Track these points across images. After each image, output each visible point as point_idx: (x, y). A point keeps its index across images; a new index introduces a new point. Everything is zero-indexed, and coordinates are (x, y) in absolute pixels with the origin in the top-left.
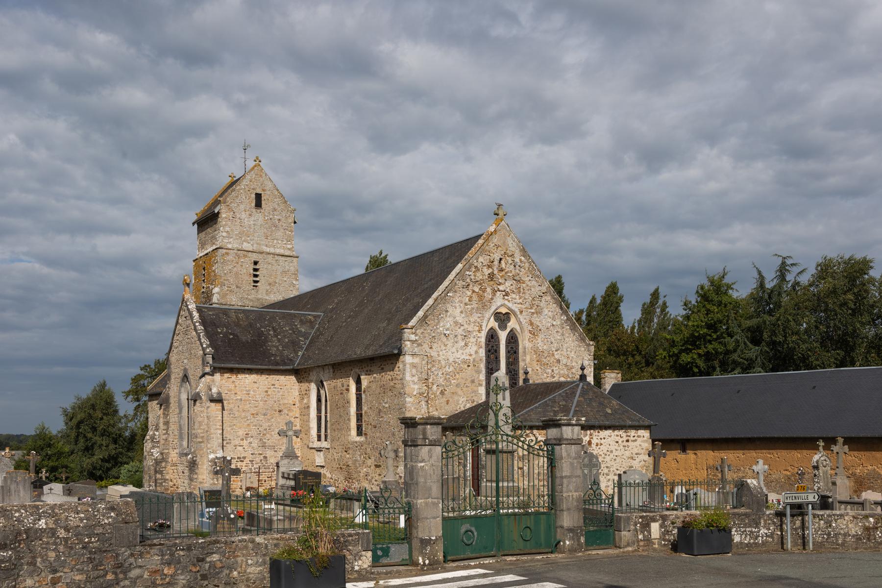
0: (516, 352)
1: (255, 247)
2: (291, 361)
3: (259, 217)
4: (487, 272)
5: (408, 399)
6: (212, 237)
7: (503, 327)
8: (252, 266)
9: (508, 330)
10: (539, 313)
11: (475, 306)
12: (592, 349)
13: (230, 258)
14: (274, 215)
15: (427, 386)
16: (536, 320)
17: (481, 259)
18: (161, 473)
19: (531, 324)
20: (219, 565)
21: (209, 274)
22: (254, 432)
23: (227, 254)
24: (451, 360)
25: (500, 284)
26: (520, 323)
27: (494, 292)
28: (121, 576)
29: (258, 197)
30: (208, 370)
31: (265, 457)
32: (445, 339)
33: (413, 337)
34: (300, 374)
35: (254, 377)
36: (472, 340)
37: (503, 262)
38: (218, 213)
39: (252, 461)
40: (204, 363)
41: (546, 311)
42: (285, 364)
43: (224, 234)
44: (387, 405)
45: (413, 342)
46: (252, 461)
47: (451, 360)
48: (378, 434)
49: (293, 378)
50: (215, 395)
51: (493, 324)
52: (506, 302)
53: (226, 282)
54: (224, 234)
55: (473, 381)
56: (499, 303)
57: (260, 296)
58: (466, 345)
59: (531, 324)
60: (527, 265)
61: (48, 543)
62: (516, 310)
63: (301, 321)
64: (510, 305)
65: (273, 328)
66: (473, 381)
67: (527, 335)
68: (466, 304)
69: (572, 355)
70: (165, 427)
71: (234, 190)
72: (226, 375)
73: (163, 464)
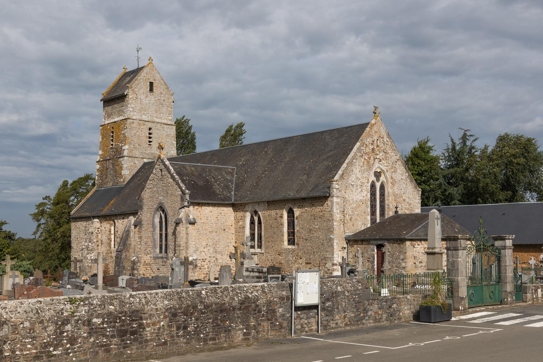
0: (384, 195)
1: (149, 119)
2: (230, 199)
3: (152, 98)
4: (371, 147)
5: (335, 223)
6: (120, 111)
7: (378, 180)
8: (148, 131)
9: (380, 182)
11: (366, 168)
12: (420, 193)
13: (134, 125)
14: (161, 97)
15: (344, 216)
17: (368, 140)
18: (137, 270)
19: (392, 178)
20: (396, 309)
21: (118, 136)
22: (210, 243)
24: (355, 200)
26: (386, 178)
27: (375, 159)
28: (365, 314)
29: (151, 84)
30: (186, 204)
31: (217, 259)
32: (352, 187)
33: (337, 187)
34: (236, 207)
35: (210, 208)
36: (365, 188)
37: (378, 141)
38: (127, 94)
39: (209, 261)
40: (182, 199)
41: (399, 171)
42: (227, 200)
43: (131, 109)
44: (317, 227)
45: (337, 189)
46: (209, 261)
47: (355, 200)
48: (308, 244)
49: (231, 209)
50: (192, 220)
51: (374, 179)
52: (380, 165)
53: (132, 142)
54: (131, 109)
55: (365, 213)
56: (377, 167)
57: (153, 152)
58: (362, 191)
59: (392, 178)
60: (390, 143)
61: (342, 298)
62: (385, 170)
63: (225, 172)
64: (382, 167)
65: (213, 177)
66: (365, 213)
67: (390, 185)
68: (361, 167)
69: (411, 196)
70: (139, 240)
71: (136, 80)
72: (196, 207)
73: (139, 264)
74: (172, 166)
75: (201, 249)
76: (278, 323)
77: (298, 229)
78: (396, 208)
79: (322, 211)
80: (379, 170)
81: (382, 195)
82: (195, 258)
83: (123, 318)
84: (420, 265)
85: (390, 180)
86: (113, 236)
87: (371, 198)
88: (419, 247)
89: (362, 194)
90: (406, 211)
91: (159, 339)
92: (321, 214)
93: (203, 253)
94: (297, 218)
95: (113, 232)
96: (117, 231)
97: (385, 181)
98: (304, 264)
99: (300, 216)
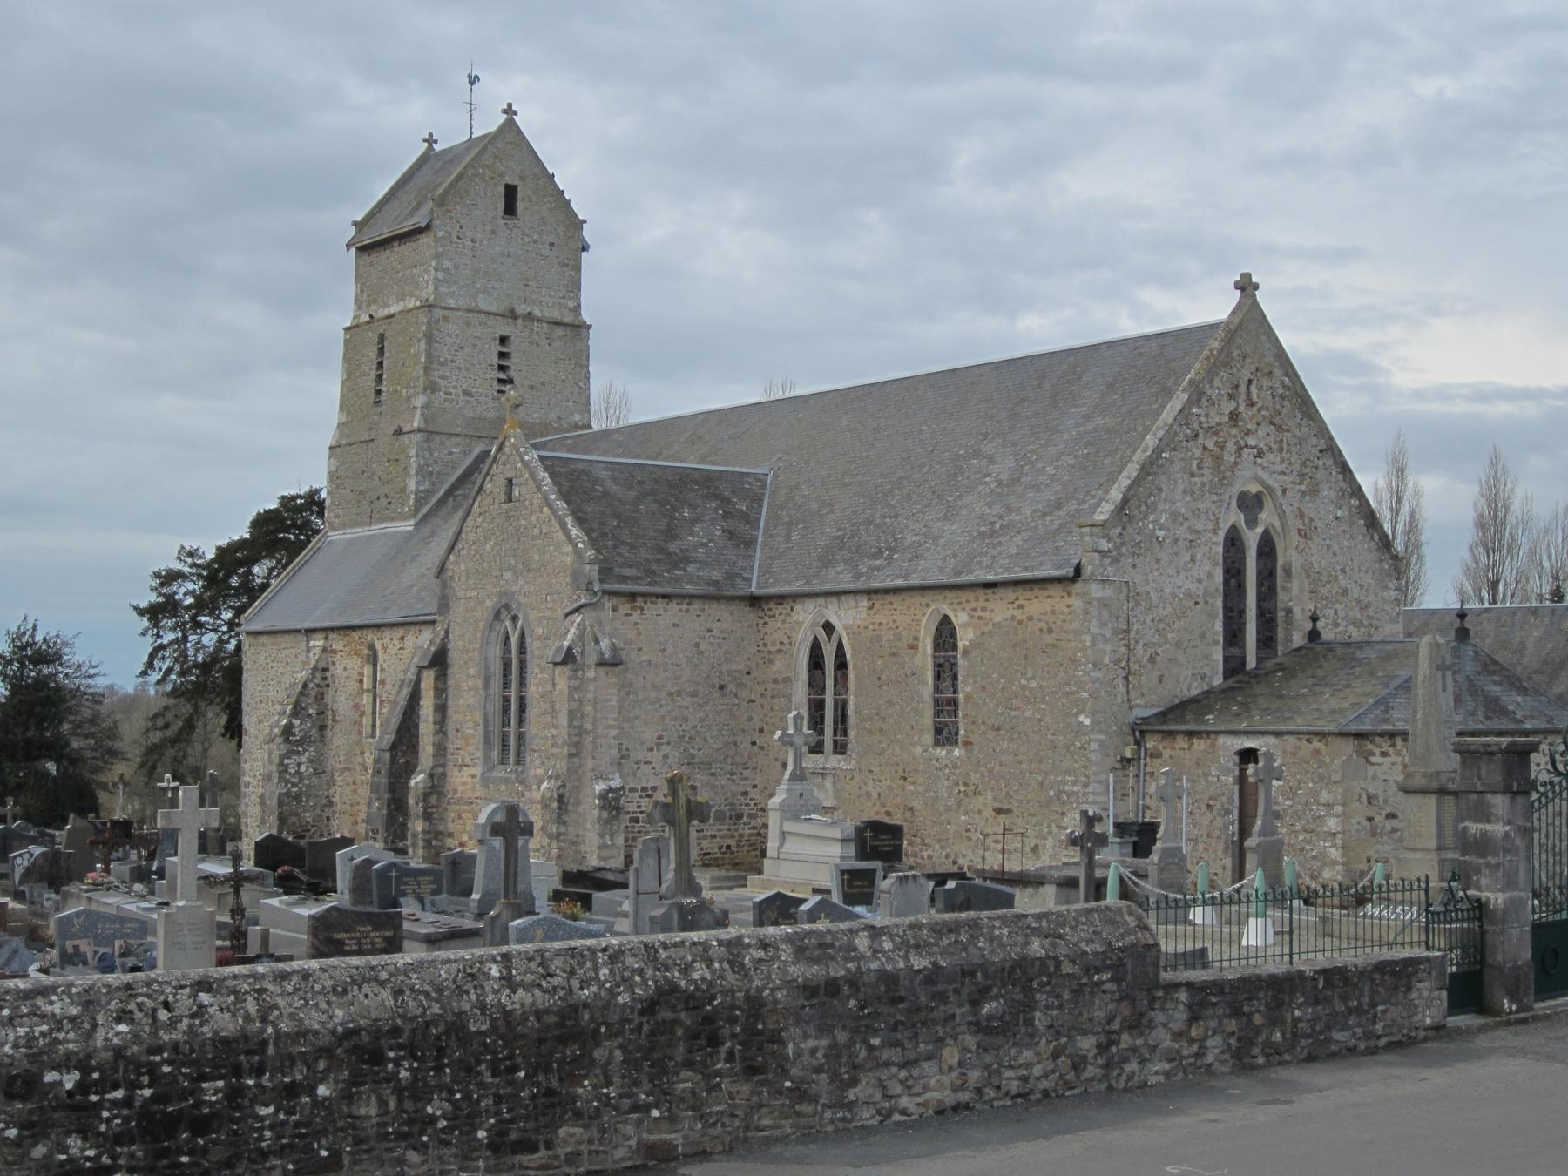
7: (1252, 522)
9: (1260, 530)
10: (1314, 492)
15: (1127, 646)
16: (1310, 509)
19: (1302, 515)
23: (446, 319)
25: (1248, 433)
26: (1282, 516)
27: (1239, 449)
29: (511, 192)
37: (1253, 388)
44: (1033, 684)
51: (1236, 517)
52: (1260, 473)
55: (1203, 636)
58: (1193, 560)
62: (1276, 485)
66: (1203, 636)
67: (1295, 539)
68: (1192, 475)
74: (546, 468)
75: (640, 754)
76: (788, 1084)
77: (969, 689)
78: (1314, 619)
79: (1050, 631)
80: (1254, 488)
81: (1267, 576)
82: (615, 784)
83: (166, 1069)
84: (1389, 825)
85: (1294, 523)
86: (367, 699)
87: (1226, 583)
88: (1387, 760)
89: (1194, 572)
90: (1351, 628)
91: (308, 1149)
92: (1049, 639)
93: (645, 768)
94: (966, 653)
95: (367, 684)
96: (383, 682)
97: (1277, 524)
98: (988, 813)
99: (975, 645)
